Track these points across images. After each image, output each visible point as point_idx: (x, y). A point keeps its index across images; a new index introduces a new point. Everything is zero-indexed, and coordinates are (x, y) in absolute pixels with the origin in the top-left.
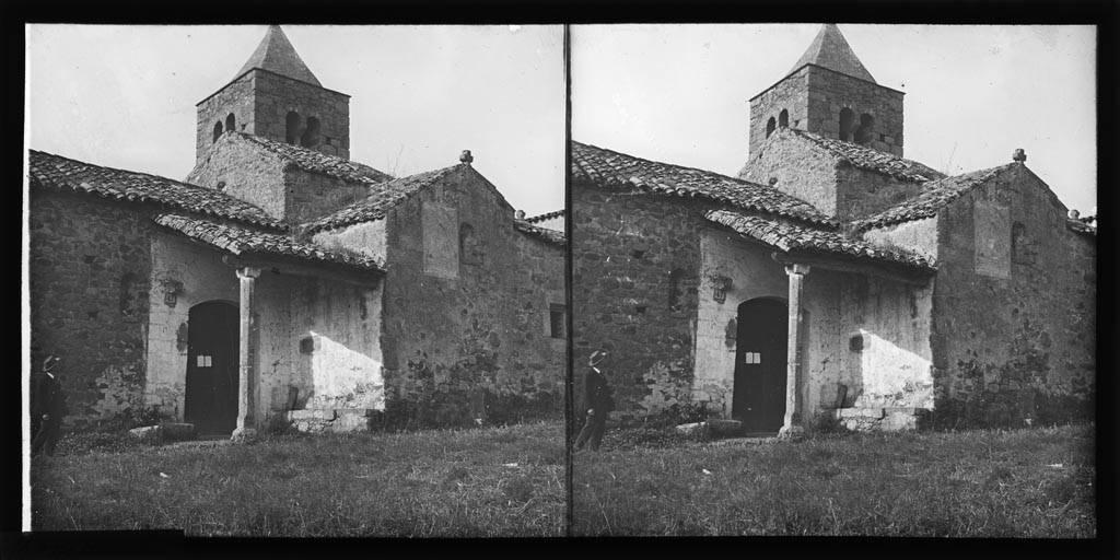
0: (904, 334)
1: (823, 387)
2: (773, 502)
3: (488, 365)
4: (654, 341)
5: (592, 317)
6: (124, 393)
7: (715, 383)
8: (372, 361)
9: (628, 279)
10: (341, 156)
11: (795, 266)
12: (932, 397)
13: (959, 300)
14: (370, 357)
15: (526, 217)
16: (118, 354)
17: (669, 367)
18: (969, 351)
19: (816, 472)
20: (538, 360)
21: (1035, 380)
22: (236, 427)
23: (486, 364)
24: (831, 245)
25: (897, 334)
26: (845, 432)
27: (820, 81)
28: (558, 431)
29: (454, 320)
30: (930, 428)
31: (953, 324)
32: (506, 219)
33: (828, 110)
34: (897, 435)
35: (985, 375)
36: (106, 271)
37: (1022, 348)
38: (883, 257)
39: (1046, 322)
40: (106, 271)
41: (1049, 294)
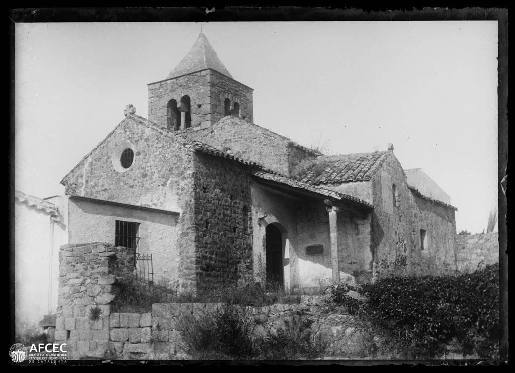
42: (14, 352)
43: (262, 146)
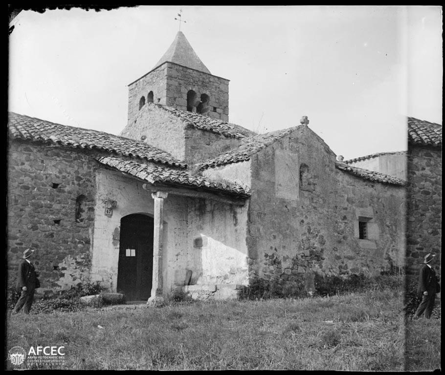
0: (229, 237)
1: (177, 271)
2: (144, 346)
3: (317, 256)
4: (65, 242)
5: (25, 227)
6: (77, 273)
7: (106, 269)
8: (240, 253)
9: (49, 202)
10: (223, 120)
11: (158, 193)
12: (247, 278)
13: (265, 215)
14: (240, 250)
15: (344, 160)
16: (74, 248)
17: (76, 259)
18: (271, 248)
19: (172, 327)
20: (351, 254)
21: (315, 266)
22: (150, 296)
23: (316, 256)
24: (182, 179)
25: (225, 237)
26: (191, 301)
27: (174, 73)
28: (361, 300)
29: (295, 226)
30: (246, 297)
31: (261, 230)
32: (330, 162)
33: (179, 92)
34: (225, 302)
35: (282, 263)
36: (66, 194)
37: (307, 246)
38: (215, 187)
39: (322, 228)
40: (66, 194)
41: (325, 211)
42: (13, 355)
43: (167, 131)
